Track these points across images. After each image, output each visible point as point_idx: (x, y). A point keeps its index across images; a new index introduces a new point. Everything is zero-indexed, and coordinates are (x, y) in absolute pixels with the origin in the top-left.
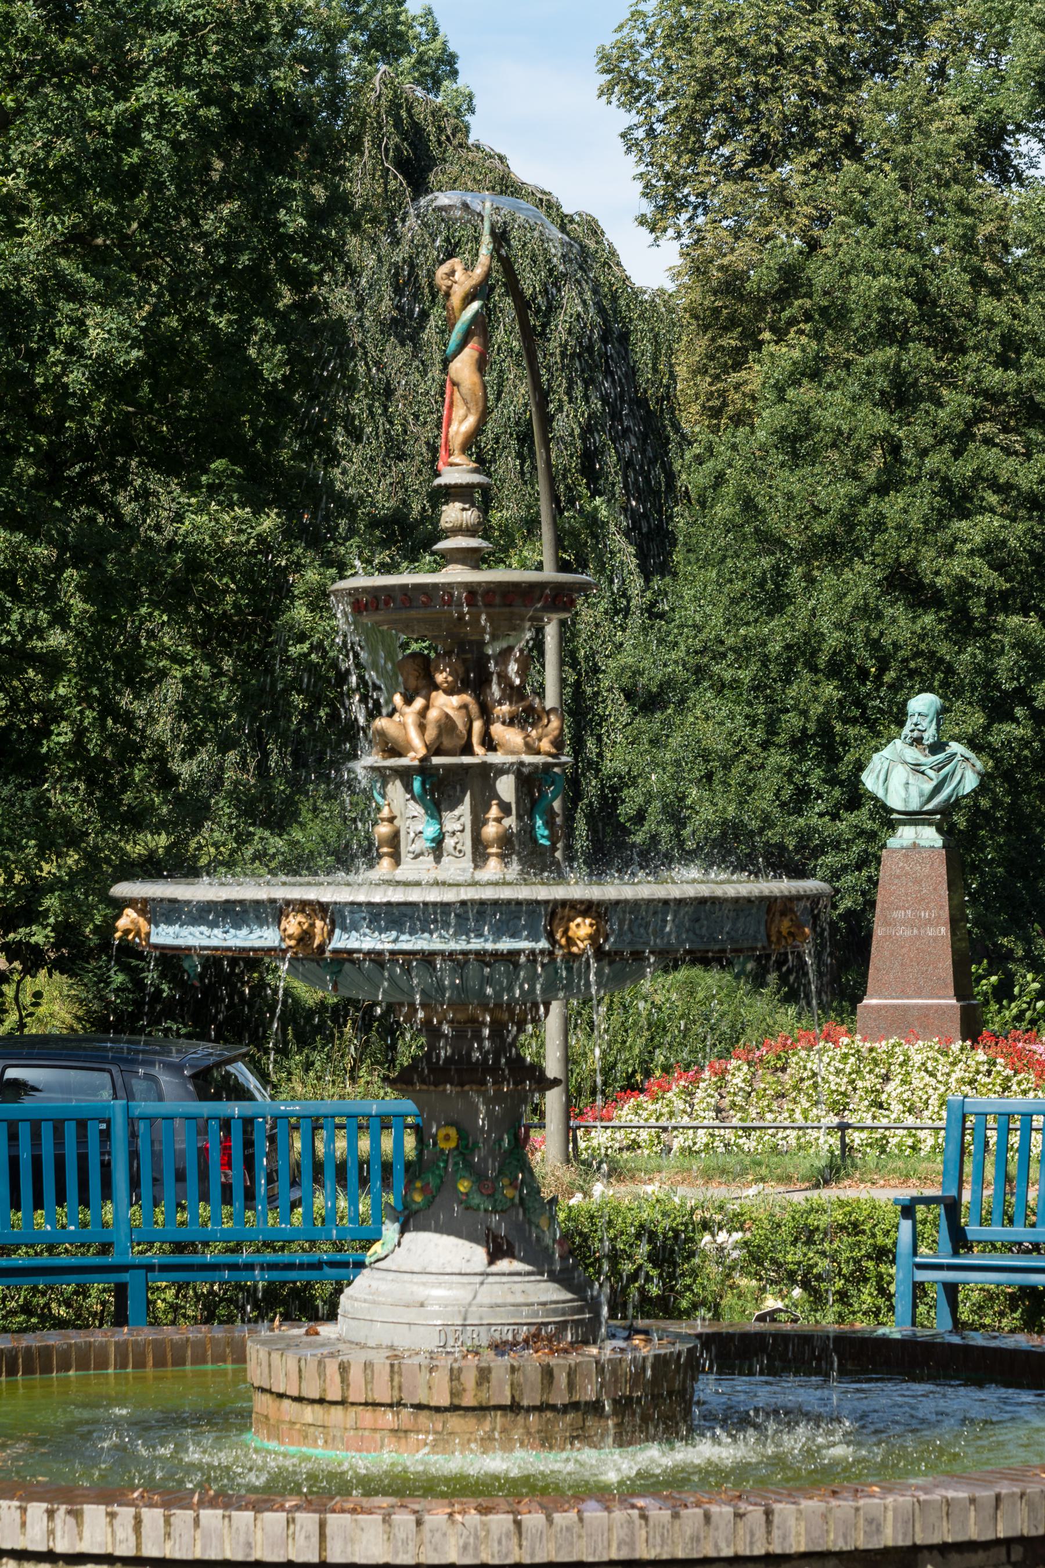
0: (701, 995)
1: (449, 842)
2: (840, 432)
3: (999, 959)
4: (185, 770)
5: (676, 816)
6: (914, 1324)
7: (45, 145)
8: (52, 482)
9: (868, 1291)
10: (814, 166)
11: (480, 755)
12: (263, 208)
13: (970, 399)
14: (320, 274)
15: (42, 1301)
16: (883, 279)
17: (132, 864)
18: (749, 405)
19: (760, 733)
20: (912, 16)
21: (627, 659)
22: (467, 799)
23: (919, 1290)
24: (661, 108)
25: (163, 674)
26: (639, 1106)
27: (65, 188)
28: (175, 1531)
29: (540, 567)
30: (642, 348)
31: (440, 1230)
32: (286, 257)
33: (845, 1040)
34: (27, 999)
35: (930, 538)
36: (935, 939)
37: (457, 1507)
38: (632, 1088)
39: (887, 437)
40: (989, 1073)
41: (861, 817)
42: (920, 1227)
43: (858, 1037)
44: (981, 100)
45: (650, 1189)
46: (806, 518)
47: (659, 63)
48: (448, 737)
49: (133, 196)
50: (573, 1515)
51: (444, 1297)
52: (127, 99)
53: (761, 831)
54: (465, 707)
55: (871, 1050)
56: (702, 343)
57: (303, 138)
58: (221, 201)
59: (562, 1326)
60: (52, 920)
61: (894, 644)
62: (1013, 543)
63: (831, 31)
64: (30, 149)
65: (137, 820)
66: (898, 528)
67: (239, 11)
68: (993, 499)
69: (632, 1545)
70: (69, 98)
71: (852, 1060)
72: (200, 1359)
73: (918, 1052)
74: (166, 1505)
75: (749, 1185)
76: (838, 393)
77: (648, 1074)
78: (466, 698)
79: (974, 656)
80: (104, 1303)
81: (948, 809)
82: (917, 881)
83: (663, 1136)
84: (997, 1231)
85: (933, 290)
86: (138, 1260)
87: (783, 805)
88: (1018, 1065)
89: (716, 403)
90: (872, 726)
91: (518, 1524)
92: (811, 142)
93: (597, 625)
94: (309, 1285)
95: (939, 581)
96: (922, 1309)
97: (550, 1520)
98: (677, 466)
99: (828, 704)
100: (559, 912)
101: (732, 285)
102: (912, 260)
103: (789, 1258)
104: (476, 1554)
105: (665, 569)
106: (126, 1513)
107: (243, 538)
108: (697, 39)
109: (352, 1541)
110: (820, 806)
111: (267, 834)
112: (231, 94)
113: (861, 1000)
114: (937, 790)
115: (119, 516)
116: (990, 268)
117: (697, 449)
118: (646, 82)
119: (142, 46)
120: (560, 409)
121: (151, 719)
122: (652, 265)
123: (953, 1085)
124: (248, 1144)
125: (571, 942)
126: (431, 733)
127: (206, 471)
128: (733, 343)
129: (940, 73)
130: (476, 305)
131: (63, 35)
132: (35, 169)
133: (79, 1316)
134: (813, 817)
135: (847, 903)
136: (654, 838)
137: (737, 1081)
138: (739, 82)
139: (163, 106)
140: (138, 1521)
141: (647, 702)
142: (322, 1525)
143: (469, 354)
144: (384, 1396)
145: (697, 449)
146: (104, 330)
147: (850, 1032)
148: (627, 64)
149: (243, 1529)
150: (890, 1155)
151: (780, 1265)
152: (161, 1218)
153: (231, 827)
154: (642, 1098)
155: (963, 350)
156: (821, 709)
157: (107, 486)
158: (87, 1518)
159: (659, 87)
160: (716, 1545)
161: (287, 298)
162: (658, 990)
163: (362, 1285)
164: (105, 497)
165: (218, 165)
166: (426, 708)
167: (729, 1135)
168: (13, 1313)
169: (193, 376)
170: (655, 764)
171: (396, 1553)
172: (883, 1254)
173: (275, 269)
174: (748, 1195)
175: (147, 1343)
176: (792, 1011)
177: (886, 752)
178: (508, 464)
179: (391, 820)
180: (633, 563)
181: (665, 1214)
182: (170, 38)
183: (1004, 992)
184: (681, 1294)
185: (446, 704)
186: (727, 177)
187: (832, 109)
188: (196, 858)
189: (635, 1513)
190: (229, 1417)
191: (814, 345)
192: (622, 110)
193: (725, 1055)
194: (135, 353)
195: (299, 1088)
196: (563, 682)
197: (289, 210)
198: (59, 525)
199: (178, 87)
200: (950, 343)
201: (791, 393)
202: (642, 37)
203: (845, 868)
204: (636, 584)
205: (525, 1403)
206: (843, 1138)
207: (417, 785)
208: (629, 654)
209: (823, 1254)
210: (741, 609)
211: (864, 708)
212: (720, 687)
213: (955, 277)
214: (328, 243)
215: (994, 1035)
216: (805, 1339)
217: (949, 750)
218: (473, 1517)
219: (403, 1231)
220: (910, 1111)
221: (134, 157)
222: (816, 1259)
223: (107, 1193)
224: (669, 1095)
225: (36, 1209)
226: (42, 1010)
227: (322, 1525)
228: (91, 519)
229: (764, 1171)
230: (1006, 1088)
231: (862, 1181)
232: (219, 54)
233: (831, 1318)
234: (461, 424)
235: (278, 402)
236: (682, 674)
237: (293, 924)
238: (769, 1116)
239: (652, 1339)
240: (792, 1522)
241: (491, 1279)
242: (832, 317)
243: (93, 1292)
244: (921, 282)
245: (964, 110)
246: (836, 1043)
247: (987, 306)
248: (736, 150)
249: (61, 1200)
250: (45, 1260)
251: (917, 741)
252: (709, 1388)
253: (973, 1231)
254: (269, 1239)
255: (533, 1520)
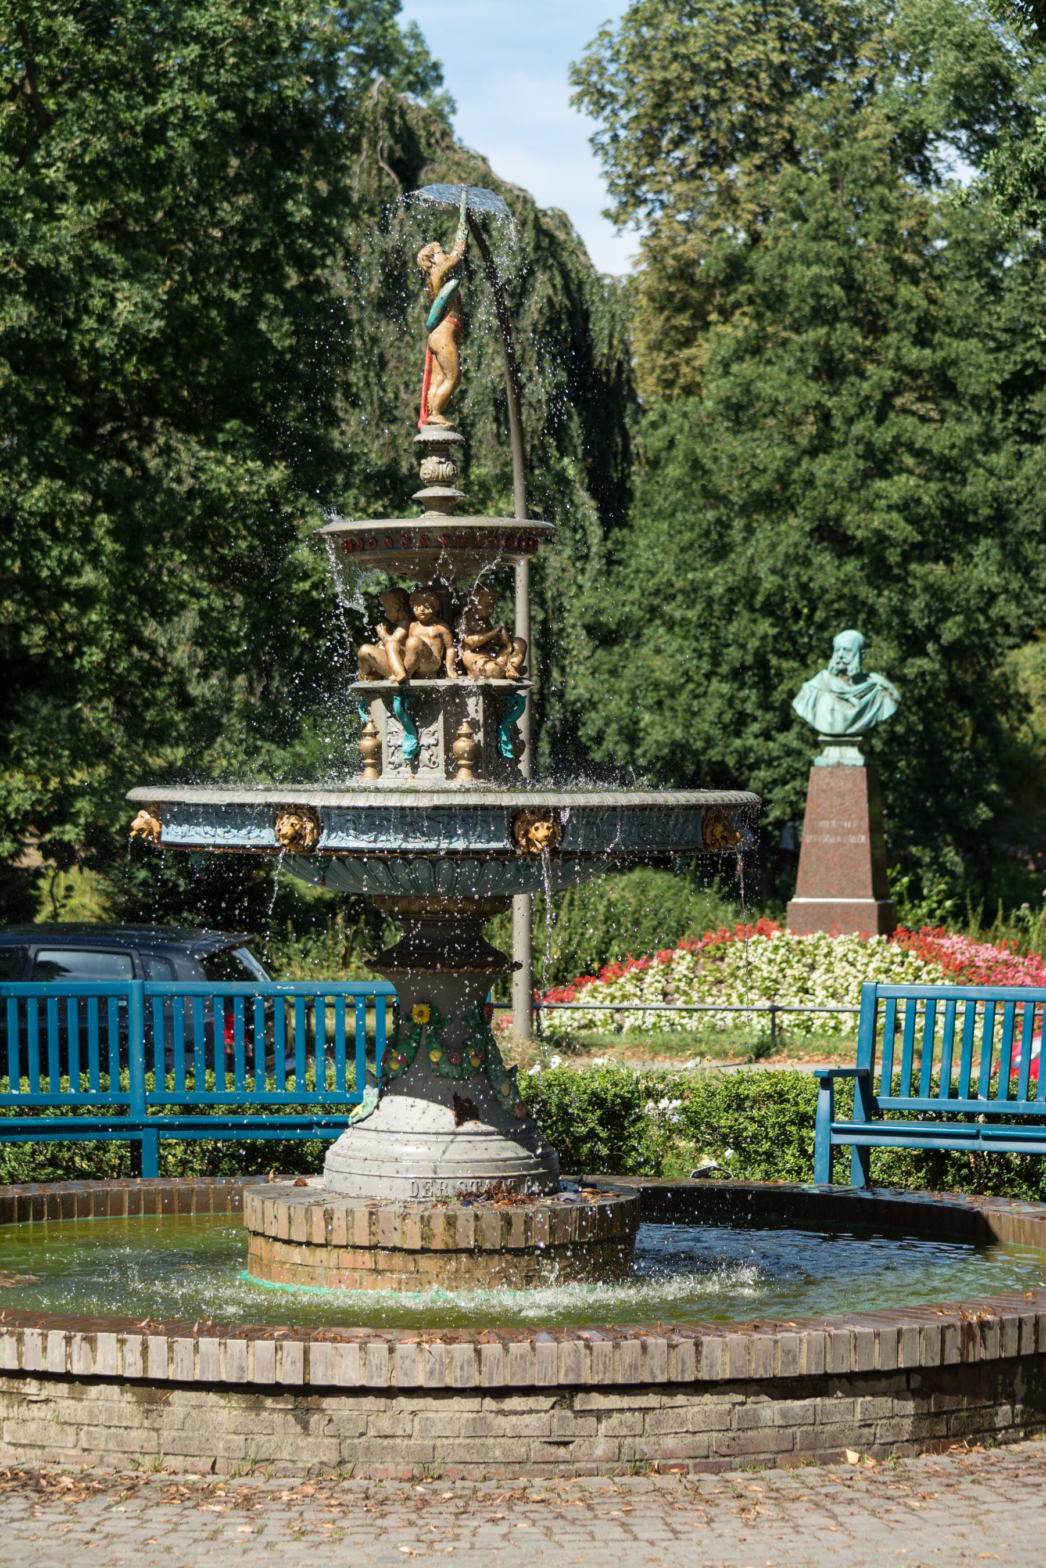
0: (652, 894)
1: (425, 755)
2: (777, 402)
3: (911, 865)
4: (195, 690)
5: (632, 736)
6: (830, 1181)
7: (82, 143)
8: (85, 438)
9: (792, 1151)
10: (759, 168)
11: (452, 678)
12: (273, 201)
13: (890, 373)
14: (323, 257)
15: (67, 1155)
16: (816, 269)
17: (152, 773)
18: (698, 378)
19: (706, 666)
20: (844, 38)
21: (588, 599)
22: (441, 717)
23: (835, 1152)
24: (625, 116)
25: (182, 606)
26: (595, 990)
27: (99, 182)
28: (177, 1358)
29: (512, 515)
30: (599, 327)
31: (413, 1092)
32: (293, 242)
33: (776, 934)
34: (61, 892)
35: (854, 496)
36: (856, 846)
37: (425, 1338)
38: (589, 974)
39: (819, 405)
40: (902, 963)
41: (790, 738)
42: (837, 1097)
43: (788, 931)
44: (905, 112)
45: (599, 1061)
46: (747, 478)
47: (622, 77)
48: (428, 662)
49: (159, 188)
50: (526, 1345)
51: (418, 1154)
52: (154, 103)
53: (705, 750)
54: (439, 636)
55: (799, 942)
56: (658, 323)
57: (309, 138)
58: (236, 193)
59: (520, 1180)
60: (82, 821)
61: (821, 588)
62: (926, 499)
63: (774, 49)
64: (69, 146)
65: (159, 735)
66: (826, 486)
67: (253, 28)
68: (909, 461)
69: (578, 1371)
70: (105, 102)
71: (782, 951)
72: (203, 1208)
73: (841, 944)
74: (170, 1333)
75: (687, 1060)
76: (776, 368)
77: (604, 962)
78: (441, 628)
79: (890, 599)
80: (121, 1158)
81: (869, 732)
82: (841, 795)
83: (617, 1016)
84: (905, 1101)
85: (859, 278)
86: (150, 1120)
87: (725, 727)
88: (928, 957)
89: (670, 376)
90: (803, 660)
91: (478, 1352)
92: (753, 146)
93: (563, 570)
94: (301, 1143)
95: (859, 534)
96: (838, 1168)
97: (506, 1349)
98: (633, 431)
99: (764, 638)
100: (515, 819)
101: (684, 272)
102: (841, 252)
103: (723, 1123)
104: (441, 1380)
105: (623, 522)
106: (134, 1341)
107: (255, 488)
108: (656, 56)
109: (333, 1366)
110: (755, 727)
111: (273, 747)
112: (246, 100)
113: (790, 898)
114: (859, 715)
115: (145, 469)
116: (909, 258)
117: (652, 416)
118: (611, 94)
119: (169, 57)
120: (530, 379)
121: (171, 648)
122: (614, 254)
123: (871, 973)
124: (249, 1019)
125: (530, 842)
126: (410, 658)
127: (222, 430)
128: (685, 323)
129: (870, 88)
130: (452, 283)
131: (100, 47)
132: (73, 164)
133: (99, 1169)
134: (749, 738)
135: (775, 813)
136: (611, 756)
137: (681, 968)
138: (691, 94)
139: (186, 109)
140: (145, 1347)
141: (604, 636)
142: (306, 1352)
143: (446, 326)
144: (363, 1240)
145: (652, 416)
146: (132, 303)
147: (782, 927)
148: (594, 78)
149: (237, 1355)
150: (814, 1035)
151: (714, 1129)
152: (171, 1083)
153: (241, 741)
154: (598, 983)
155: (886, 331)
156: (757, 643)
157: (135, 443)
158: (100, 1344)
159: (622, 98)
160: (652, 1372)
161: (293, 279)
162: (618, 889)
163: (345, 1144)
164: (132, 452)
165: (234, 162)
166: (406, 637)
167: (673, 1015)
168: (42, 1166)
169: (210, 345)
170: (612, 691)
171: (371, 1377)
172: (805, 1120)
173: (276, 251)
174: (687, 1068)
175: (157, 1192)
176: (731, 908)
177: (814, 682)
178: (485, 428)
179: (374, 735)
180: (594, 516)
181: (615, 1084)
182: (193, 51)
183: (915, 892)
184: (628, 1153)
185: (423, 633)
186: (680, 178)
187: (774, 118)
188: (210, 769)
189: (581, 1343)
190: (224, 1258)
191: (755, 326)
192: (590, 118)
193: (672, 946)
194: (158, 323)
195: (299, 973)
196: (531, 619)
197: (296, 202)
198: (93, 475)
199: (199, 93)
200: (874, 326)
201: (735, 368)
202: (608, 54)
203: (775, 782)
204: (595, 534)
205: (488, 1246)
206: (773, 1019)
207: (396, 704)
208: (585, 596)
209: (752, 1119)
210: (688, 556)
211: (794, 643)
212: (671, 625)
213: (880, 268)
214: (330, 231)
215: (908, 930)
216: (740, 1194)
217: (870, 681)
218: (439, 1346)
219: (381, 1095)
220: (833, 996)
221: (159, 153)
222: (747, 1123)
223: (124, 1059)
224: (622, 980)
225: (61, 1074)
226: (73, 902)
227: (306, 1352)
228: (120, 472)
229: (703, 1047)
230: (917, 977)
231: (789, 1057)
232: (235, 65)
233: (758, 1175)
234: (439, 388)
235: (284, 370)
236: (638, 613)
237: (287, 825)
238: (709, 1000)
239: (599, 1189)
240: (719, 1353)
241: (459, 1138)
242: (772, 301)
243: (112, 1148)
244: (849, 272)
245: (889, 119)
246: (768, 936)
247: (906, 292)
248: (689, 153)
249: (84, 1067)
250: (70, 1119)
251: (842, 672)
252: (651, 1236)
253: (884, 1100)
254: (266, 1102)
255: (492, 1349)
